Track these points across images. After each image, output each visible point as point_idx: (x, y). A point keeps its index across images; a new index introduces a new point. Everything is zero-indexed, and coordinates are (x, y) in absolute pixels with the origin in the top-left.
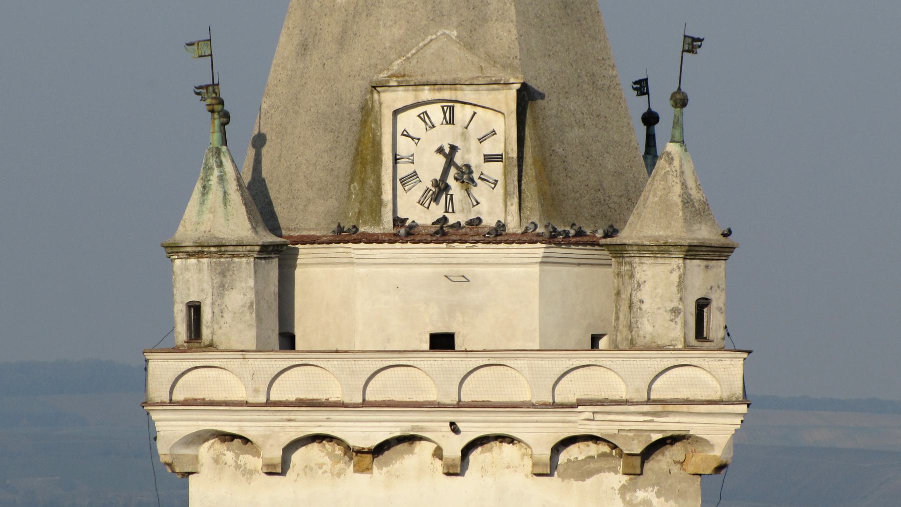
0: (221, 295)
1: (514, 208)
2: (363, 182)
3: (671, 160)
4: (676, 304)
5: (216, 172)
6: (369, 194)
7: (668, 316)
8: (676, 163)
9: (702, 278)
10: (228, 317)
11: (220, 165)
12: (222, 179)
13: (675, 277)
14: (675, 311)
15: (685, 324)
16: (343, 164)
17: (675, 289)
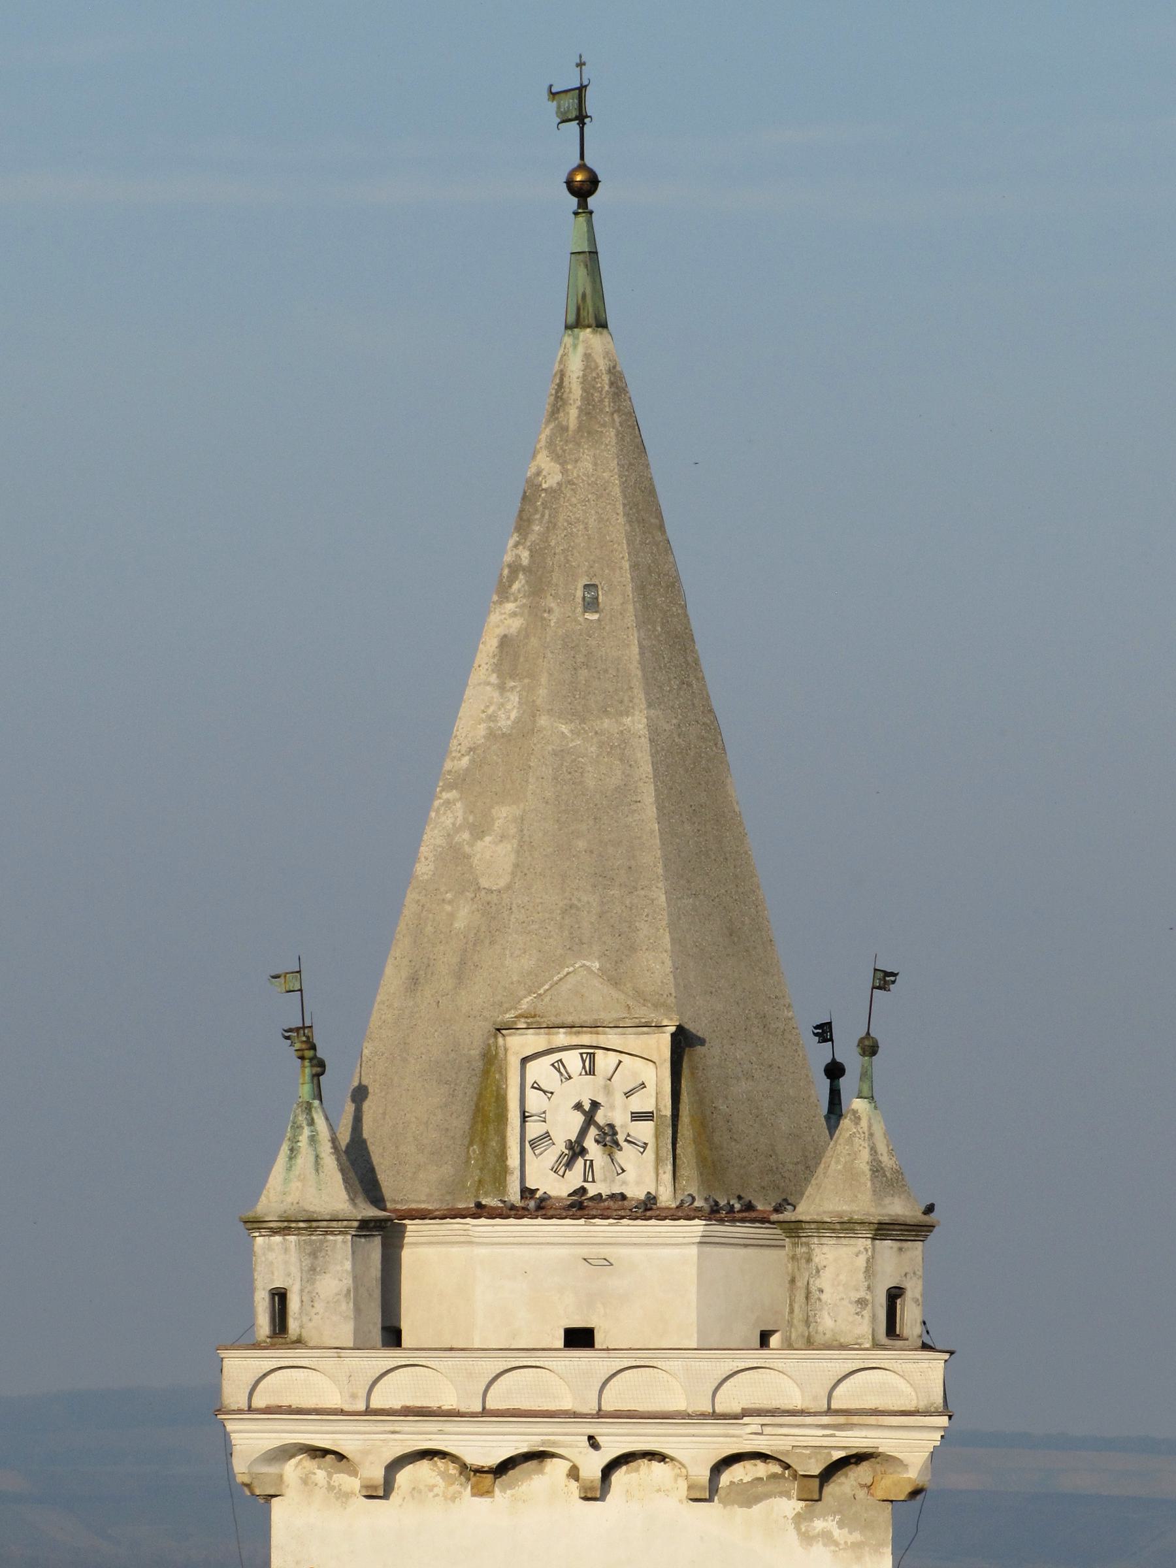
0: (311, 1281)
1: (667, 1177)
2: (484, 1144)
3: (857, 1119)
4: (862, 1294)
5: (306, 1132)
6: (492, 1159)
7: (853, 1308)
8: (864, 1123)
9: (896, 1262)
10: (319, 1306)
11: (311, 1123)
12: (313, 1140)
13: (861, 1261)
14: (861, 1302)
15: (874, 1318)
16: (461, 1123)
17: (861, 1276)
